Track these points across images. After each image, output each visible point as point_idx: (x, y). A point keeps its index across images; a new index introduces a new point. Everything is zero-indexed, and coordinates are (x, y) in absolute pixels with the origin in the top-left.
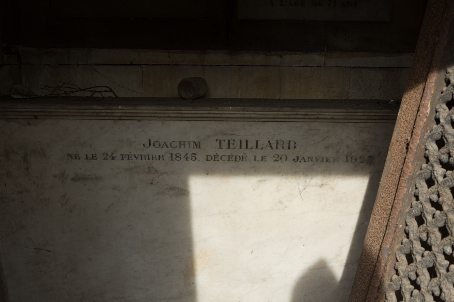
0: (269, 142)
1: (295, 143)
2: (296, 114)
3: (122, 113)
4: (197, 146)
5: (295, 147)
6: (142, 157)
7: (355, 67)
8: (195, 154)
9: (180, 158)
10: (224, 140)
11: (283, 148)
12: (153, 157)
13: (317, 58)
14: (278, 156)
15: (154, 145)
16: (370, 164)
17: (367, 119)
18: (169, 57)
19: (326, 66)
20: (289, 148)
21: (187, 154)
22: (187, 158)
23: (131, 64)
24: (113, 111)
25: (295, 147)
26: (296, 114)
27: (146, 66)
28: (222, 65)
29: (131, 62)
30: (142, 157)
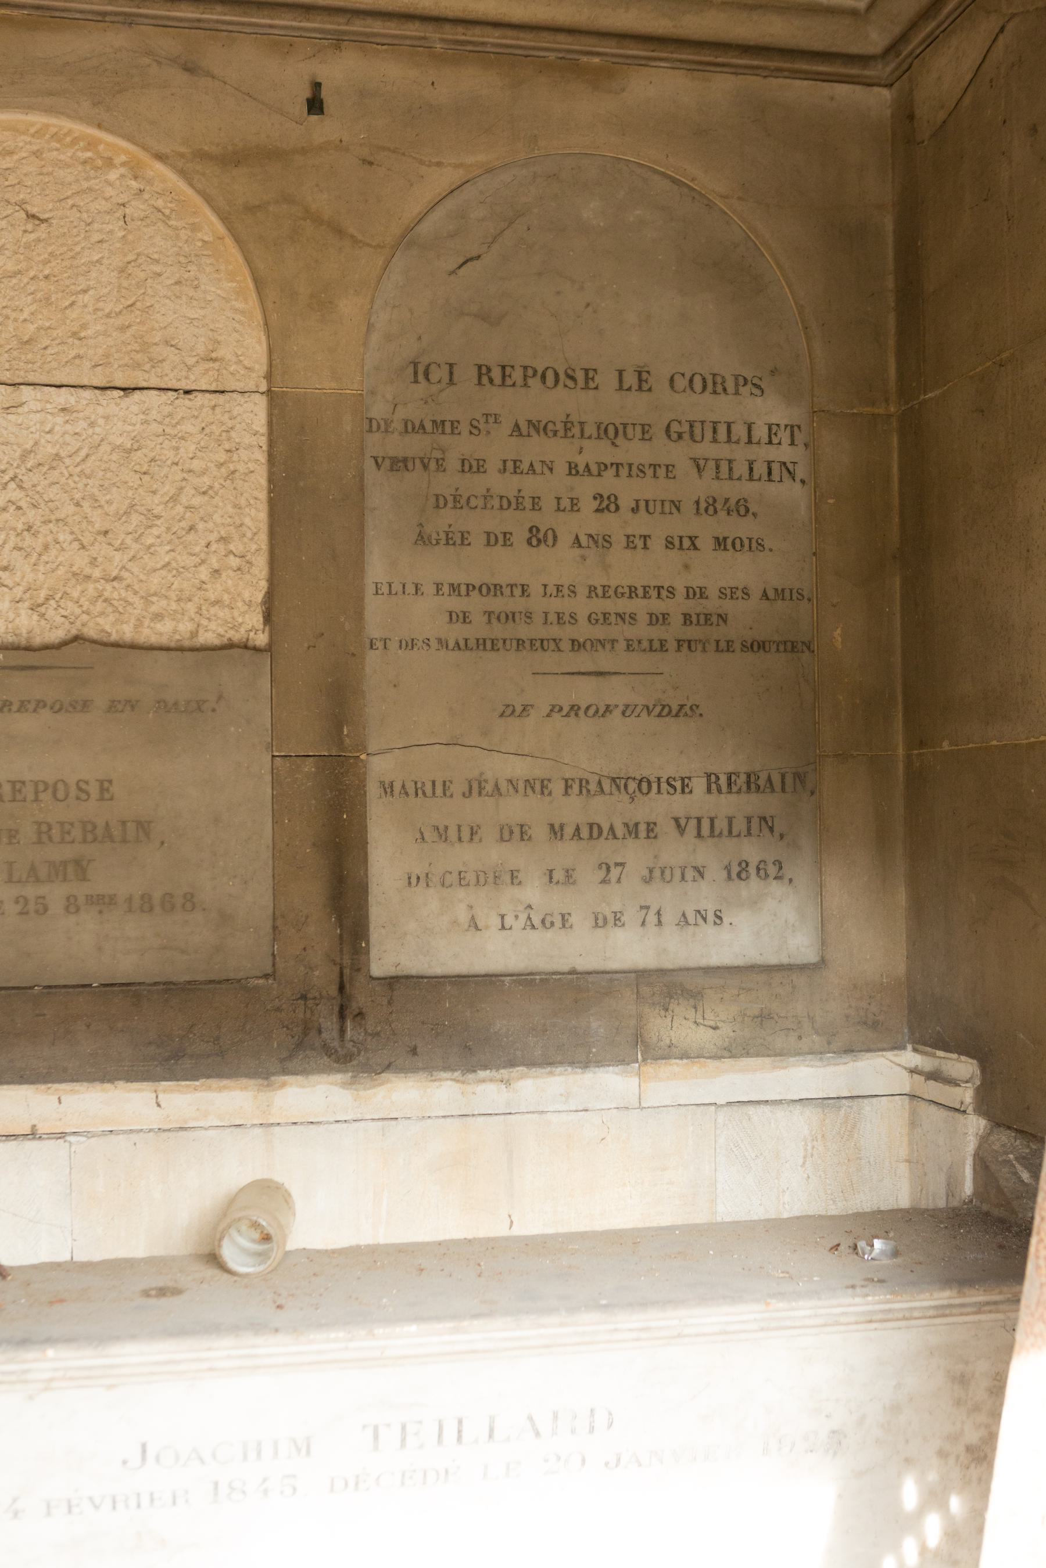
0: (530, 1418)
1: (610, 1414)
2: (616, 1330)
3: (56, 1370)
4: (299, 1450)
5: (610, 1425)
6: (114, 1502)
7: (729, 1104)
8: (294, 1476)
9: (244, 1492)
10: (388, 1425)
11: (573, 1431)
12: (152, 1500)
13: (612, 1083)
14: (559, 1458)
15: (157, 1459)
16: (835, 1453)
17: (825, 1325)
18: (159, 1105)
19: (644, 1105)
20: (592, 1430)
21: (265, 1480)
22: (266, 1492)
23: (33, 1134)
24: (26, 1366)
25: (610, 1425)
26: (616, 1330)
27: (83, 1139)
28: (328, 1123)
29: (34, 1126)
30: (114, 1502)
